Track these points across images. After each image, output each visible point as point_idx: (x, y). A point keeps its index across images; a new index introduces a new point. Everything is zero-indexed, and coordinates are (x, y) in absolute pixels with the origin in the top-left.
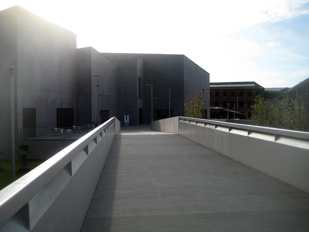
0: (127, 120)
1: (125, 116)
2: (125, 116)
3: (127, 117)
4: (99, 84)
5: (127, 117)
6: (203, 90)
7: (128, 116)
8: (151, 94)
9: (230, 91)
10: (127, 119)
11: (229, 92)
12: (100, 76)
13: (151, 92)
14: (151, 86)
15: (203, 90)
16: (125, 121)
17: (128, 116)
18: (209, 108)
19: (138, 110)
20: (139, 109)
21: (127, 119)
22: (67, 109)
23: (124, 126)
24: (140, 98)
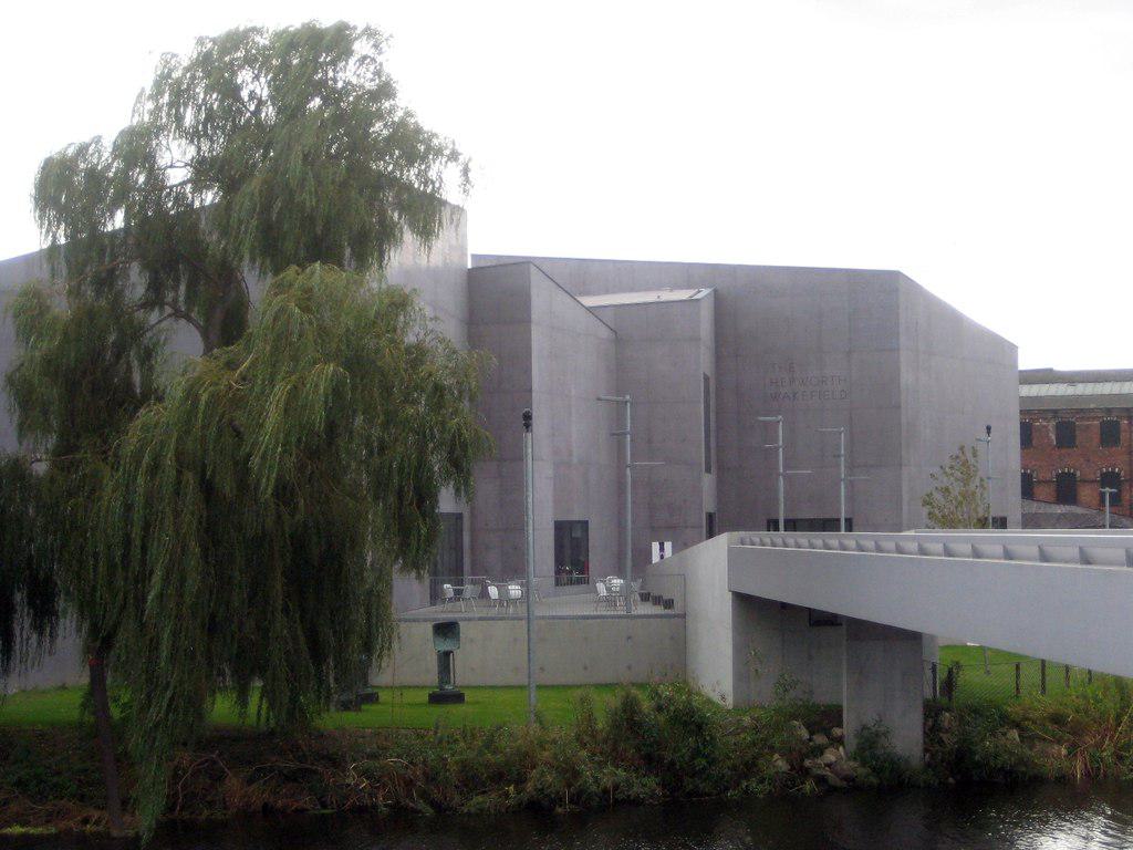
1: (655, 546)
2: (655, 546)
15: (989, 428)
17: (668, 546)
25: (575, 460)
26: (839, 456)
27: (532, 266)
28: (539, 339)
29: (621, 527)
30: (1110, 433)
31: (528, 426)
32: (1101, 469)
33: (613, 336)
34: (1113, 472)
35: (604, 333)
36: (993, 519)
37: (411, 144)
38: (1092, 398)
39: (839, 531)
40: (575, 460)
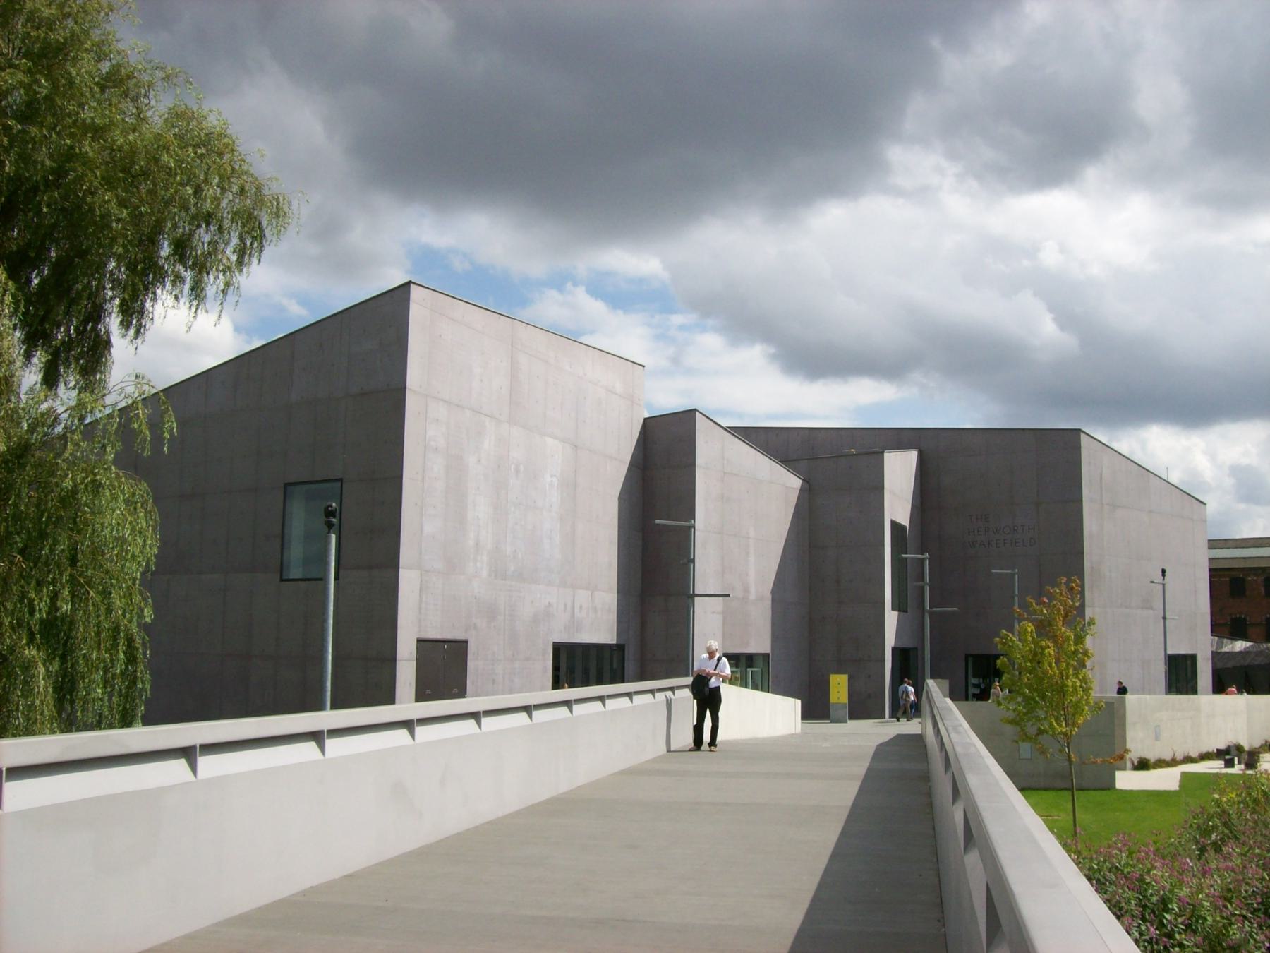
0: (839, 688)
6: (1164, 571)
15: (1164, 571)
26: (1013, 597)
40: (752, 596)
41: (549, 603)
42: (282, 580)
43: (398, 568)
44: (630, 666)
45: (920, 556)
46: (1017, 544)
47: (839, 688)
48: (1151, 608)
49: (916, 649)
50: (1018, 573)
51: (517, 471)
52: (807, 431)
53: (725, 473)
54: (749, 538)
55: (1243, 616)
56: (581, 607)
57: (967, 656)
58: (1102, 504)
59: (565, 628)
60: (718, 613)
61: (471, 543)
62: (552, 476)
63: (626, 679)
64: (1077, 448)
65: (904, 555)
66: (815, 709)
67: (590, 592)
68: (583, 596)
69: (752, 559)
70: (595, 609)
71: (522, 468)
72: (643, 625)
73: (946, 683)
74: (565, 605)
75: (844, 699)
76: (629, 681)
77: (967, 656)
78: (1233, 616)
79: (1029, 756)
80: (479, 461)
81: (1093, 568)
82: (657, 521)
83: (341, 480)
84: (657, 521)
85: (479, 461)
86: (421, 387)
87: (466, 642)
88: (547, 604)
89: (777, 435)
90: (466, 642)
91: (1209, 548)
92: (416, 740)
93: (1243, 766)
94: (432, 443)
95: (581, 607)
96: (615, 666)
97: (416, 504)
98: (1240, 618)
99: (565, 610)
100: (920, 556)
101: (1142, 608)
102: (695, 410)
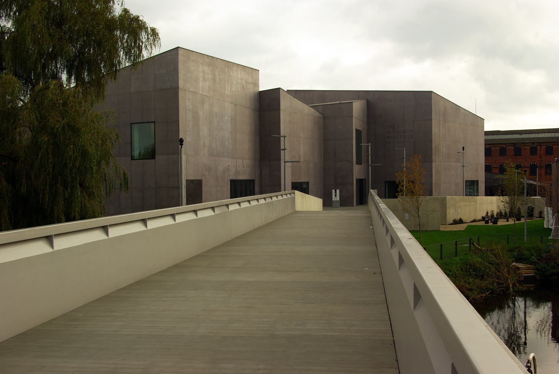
0: (336, 197)
1: (334, 191)
2: (334, 191)
3: (336, 192)
4: (285, 147)
5: (336, 192)
6: (463, 148)
7: (338, 191)
8: (404, 151)
9: (544, 146)
10: (336, 195)
11: (541, 148)
12: (286, 137)
13: (404, 150)
14: (369, 145)
15: (463, 148)
16: (333, 199)
17: (338, 191)
18: (481, 176)
19: (355, 182)
20: (357, 180)
21: (336, 195)
22: (245, 181)
23: (332, 206)
24: (359, 162)
25: (302, 160)
26: (403, 159)
27: (280, 89)
28: (284, 117)
29: (181, 190)
30: (549, 151)
31: (182, 145)
32: (530, 163)
33: (322, 116)
34: (535, 164)
35: (317, 114)
36: (466, 181)
37: (137, 19)
38: (527, 139)
39: (280, 191)
40: (302, 160)
41: (228, 165)
42: (132, 159)
43: (280, 160)
44: (257, 188)
45: (367, 144)
46: (406, 137)
47: (336, 197)
48: (460, 162)
49: (365, 179)
50: (406, 150)
51: (216, 116)
52: (321, 92)
53: (291, 112)
54: (300, 137)
55: (549, 163)
56: (239, 166)
57: (386, 182)
58: (440, 121)
59: (234, 174)
60: (290, 167)
61: (202, 144)
62: (228, 117)
63: (255, 194)
64: (431, 99)
65: (361, 144)
66: (327, 203)
67: (242, 160)
68: (240, 161)
69: (302, 145)
70: (244, 167)
71: (218, 114)
72: (261, 172)
73: (376, 191)
74: (234, 165)
75: (338, 198)
76: (256, 195)
77: (386, 182)
78: (501, 164)
79: (408, 219)
80: (203, 113)
81: (436, 147)
82: (273, 136)
83: (154, 122)
84: (273, 136)
85: (203, 113)
86: (183, 87)
87: (356, 164)
88: (228, 165)
89: (309, 93)
90: (356, 164)
91: (485, 135)
92: (148, 227)
93: (492, 223)
94: (188, 108)
95: (239, 166)
96: (251, 188)
97: (184, 130)
98: (532, 164)
99: (234, 167)
100: (367, 144)
101: (456, 162)
102: (280, 88)
